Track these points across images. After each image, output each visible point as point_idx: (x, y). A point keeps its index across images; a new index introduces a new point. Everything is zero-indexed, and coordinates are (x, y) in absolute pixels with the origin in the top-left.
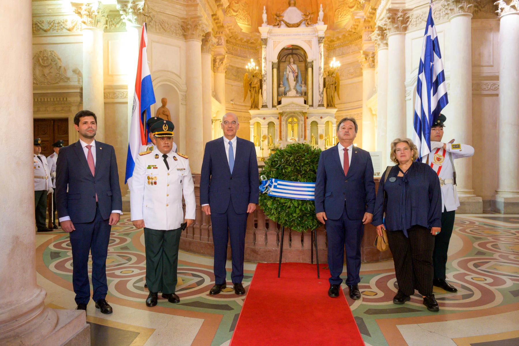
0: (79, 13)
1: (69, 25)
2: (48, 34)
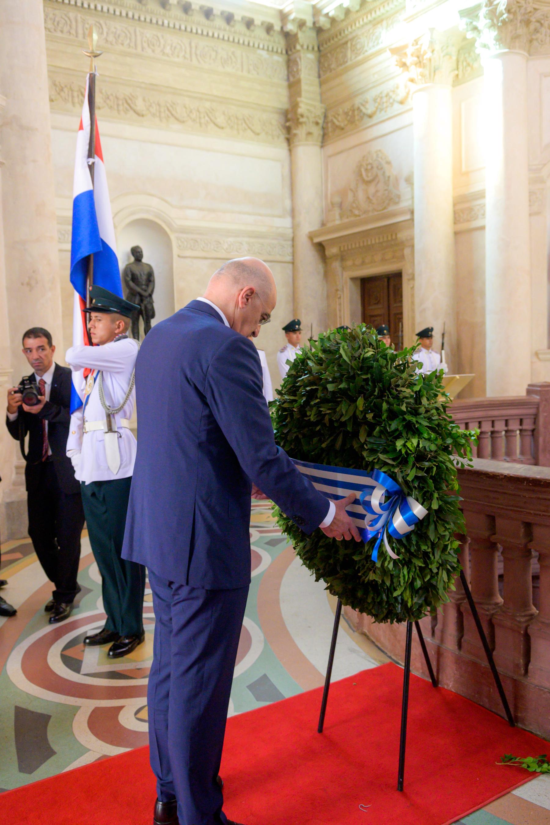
0: (404, 65)
1: (401, 94)
2: (375, 120)
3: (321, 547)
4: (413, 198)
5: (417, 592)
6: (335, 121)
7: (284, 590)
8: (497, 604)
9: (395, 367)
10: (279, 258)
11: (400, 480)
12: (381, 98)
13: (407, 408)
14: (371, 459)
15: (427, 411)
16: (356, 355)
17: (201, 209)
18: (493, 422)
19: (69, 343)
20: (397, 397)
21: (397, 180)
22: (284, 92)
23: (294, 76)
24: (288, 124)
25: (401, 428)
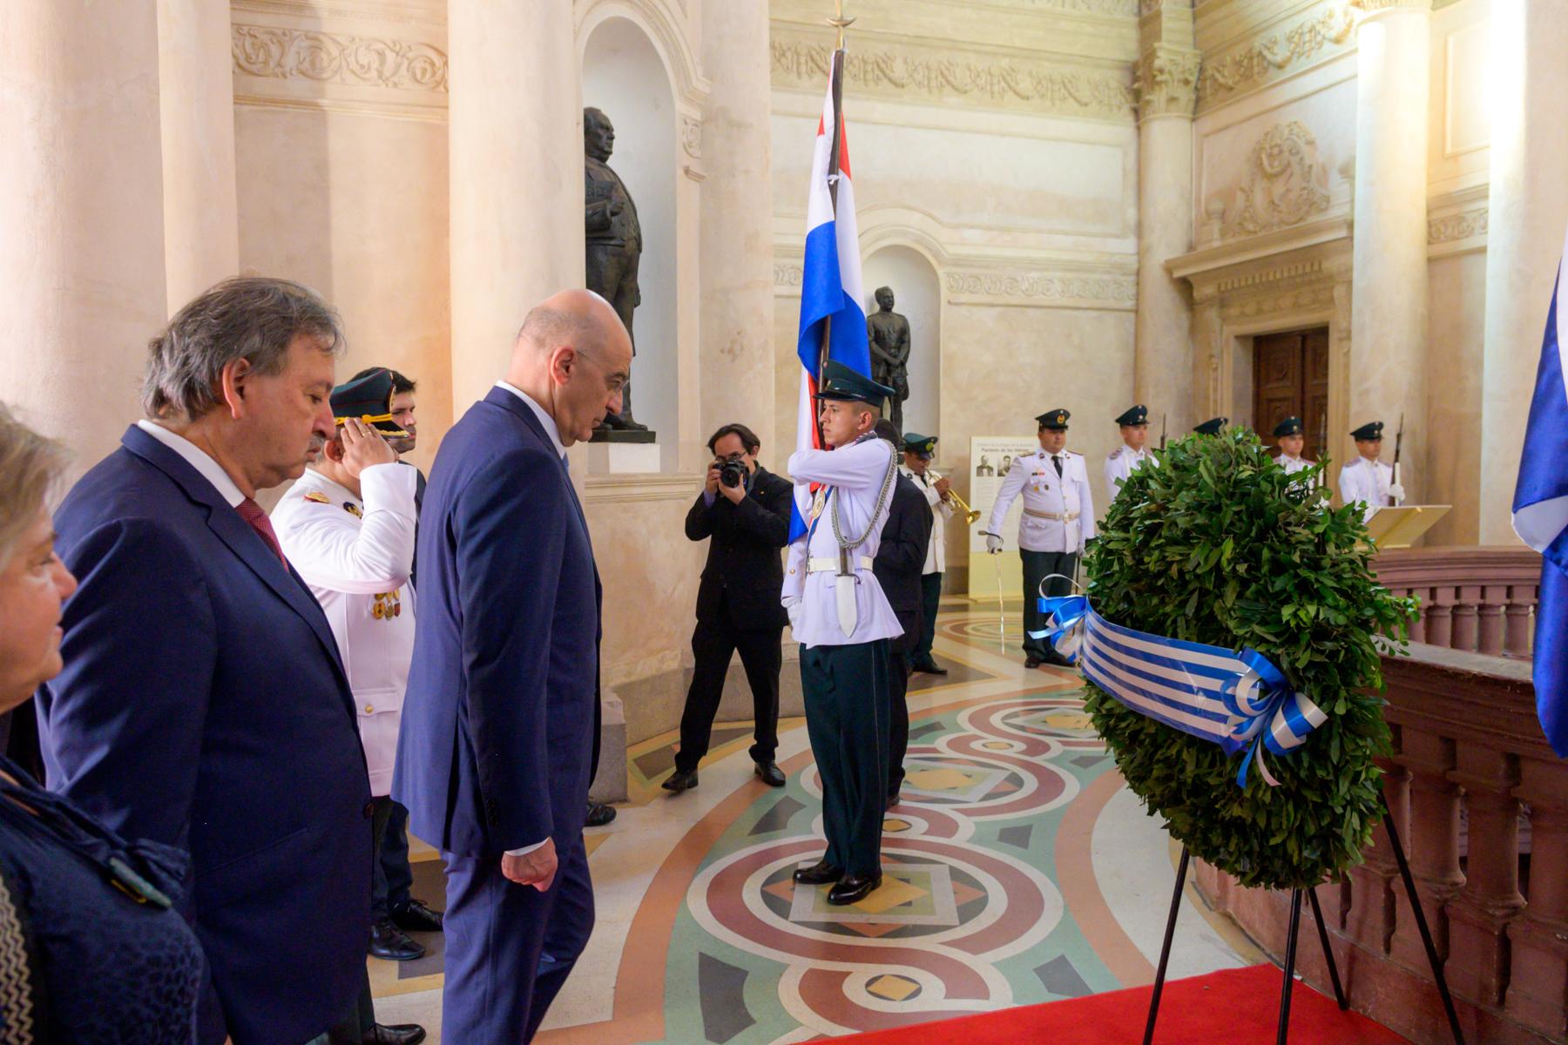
2: (1289, 71)
3: (1159, 761)
4: (1352, 201)
5: (1309, 841)
6: (1218, 76)
7: (1098, 835)
8: (1455, 884)
9: (1287, 496)
10: (1112, 303)
11: (1285, 666)
12: (1302, 34)
13: (1301, 558)
14: (1241, 632)
15: (1334, 565)
16: (1225, 475)
17: (989, 228)
18: (1483, 589)
19: (788, 441)
20: (1287, 541)
21: (1325, 171)
22: (1131, 35)
23: (1149, 7)
24: (1136, 86)
25: (1290, 588)
